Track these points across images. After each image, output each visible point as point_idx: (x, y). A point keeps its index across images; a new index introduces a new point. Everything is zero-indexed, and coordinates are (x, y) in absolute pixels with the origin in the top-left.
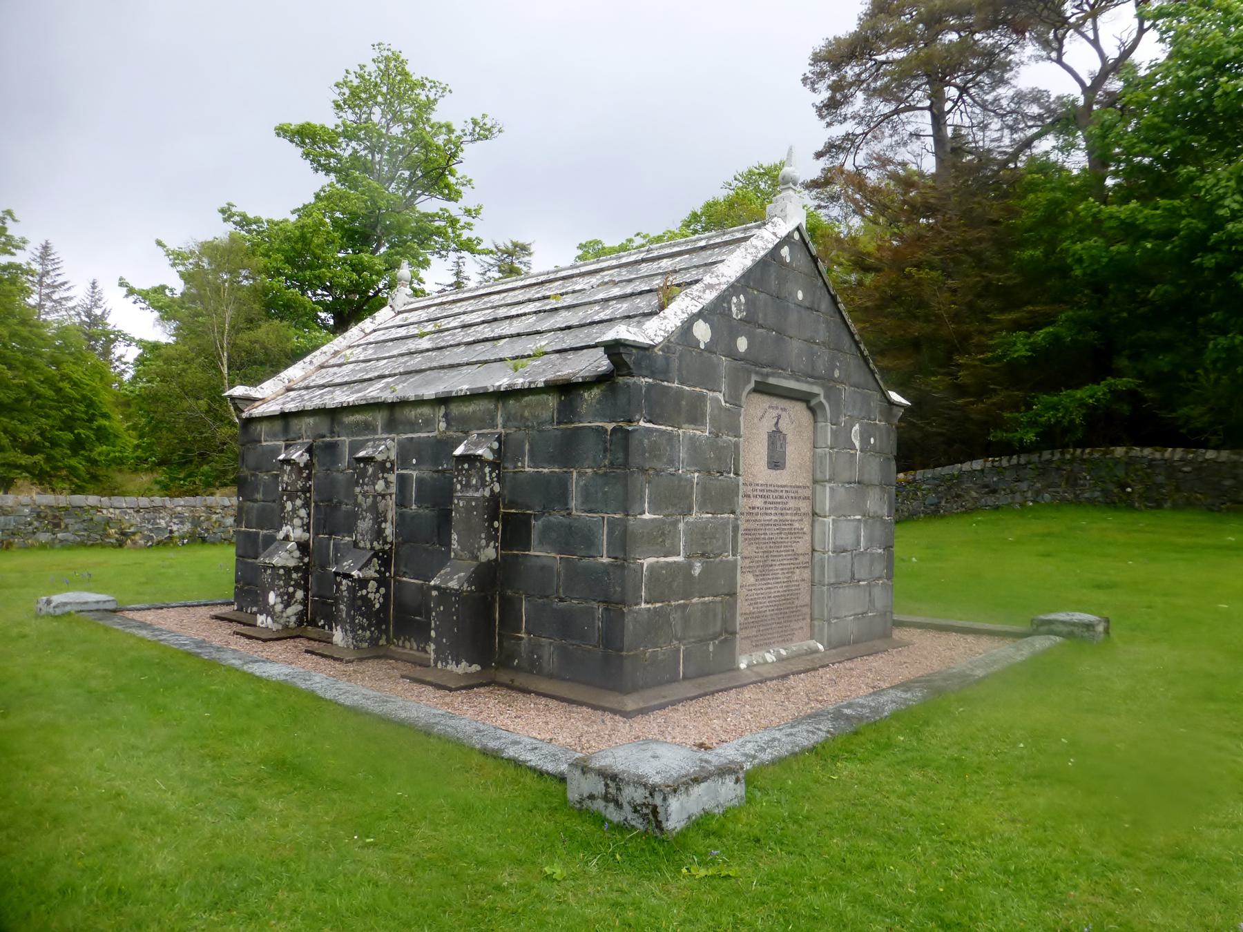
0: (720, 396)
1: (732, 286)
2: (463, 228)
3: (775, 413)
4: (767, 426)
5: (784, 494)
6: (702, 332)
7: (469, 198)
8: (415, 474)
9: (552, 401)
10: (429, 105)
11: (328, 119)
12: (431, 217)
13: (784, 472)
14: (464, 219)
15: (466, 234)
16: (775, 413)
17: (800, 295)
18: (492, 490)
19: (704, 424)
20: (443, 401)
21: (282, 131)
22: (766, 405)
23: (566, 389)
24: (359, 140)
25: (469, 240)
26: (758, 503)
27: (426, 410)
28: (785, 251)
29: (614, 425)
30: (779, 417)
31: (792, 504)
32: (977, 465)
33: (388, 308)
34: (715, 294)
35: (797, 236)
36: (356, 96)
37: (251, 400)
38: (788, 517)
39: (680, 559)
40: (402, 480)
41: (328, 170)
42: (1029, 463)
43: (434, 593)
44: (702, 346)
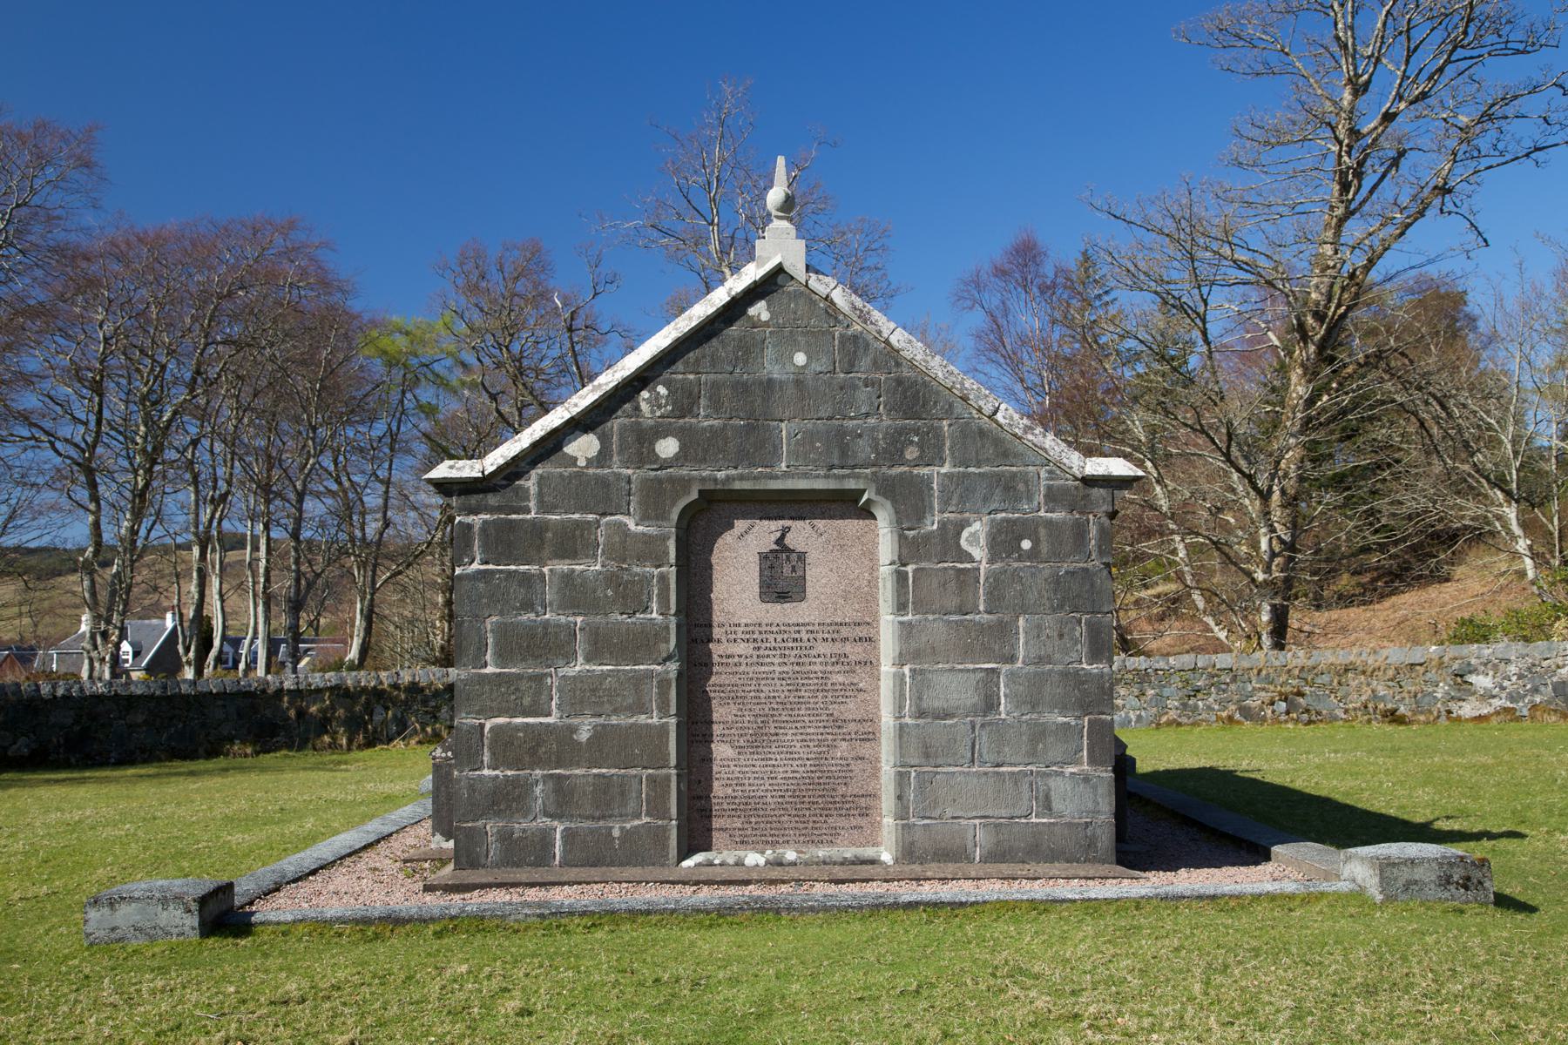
13: (803, 605)
31: (822, 648)
38: (817, 668)
44: (582, 463)
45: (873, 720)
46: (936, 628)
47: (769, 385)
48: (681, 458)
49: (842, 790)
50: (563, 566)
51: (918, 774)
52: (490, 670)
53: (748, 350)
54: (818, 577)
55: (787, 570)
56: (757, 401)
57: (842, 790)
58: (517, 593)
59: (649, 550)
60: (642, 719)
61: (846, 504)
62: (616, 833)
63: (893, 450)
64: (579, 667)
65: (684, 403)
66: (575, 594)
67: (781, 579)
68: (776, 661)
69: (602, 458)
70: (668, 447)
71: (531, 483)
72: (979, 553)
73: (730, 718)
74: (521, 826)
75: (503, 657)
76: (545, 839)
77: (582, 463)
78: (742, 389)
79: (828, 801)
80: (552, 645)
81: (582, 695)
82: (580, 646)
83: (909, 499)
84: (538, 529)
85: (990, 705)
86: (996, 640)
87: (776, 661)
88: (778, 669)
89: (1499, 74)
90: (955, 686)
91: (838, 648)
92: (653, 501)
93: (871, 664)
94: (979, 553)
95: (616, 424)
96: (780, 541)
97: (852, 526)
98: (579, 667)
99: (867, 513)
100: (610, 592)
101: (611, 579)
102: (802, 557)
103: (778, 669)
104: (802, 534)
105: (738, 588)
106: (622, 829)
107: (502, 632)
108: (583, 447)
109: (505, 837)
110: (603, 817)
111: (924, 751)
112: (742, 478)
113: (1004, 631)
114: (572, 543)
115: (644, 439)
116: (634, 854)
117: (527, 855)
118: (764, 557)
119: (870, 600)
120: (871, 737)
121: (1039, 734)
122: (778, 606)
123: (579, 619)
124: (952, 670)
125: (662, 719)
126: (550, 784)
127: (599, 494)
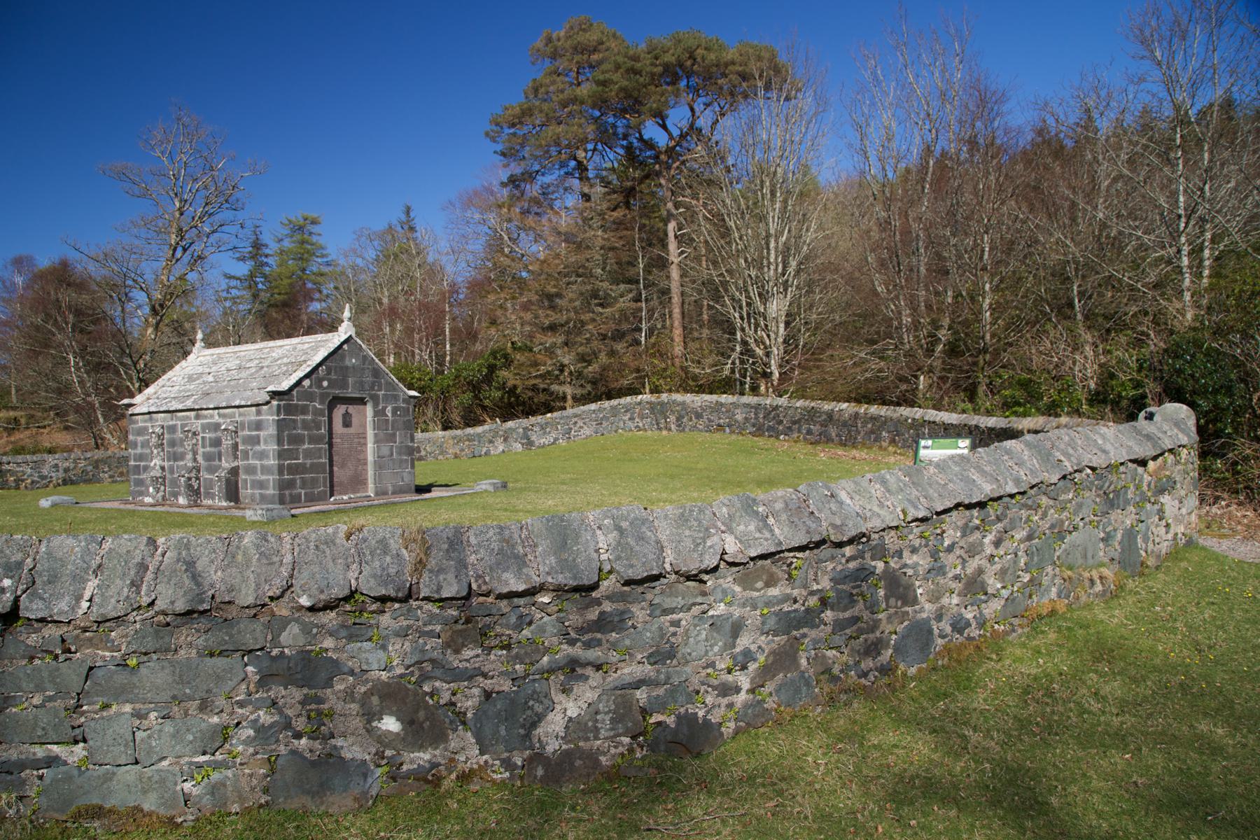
45: (366, 459)
46: (381, 434)
47: (347, 367)
48: (328, 387)
53: (343, 358)
54: (355, 421)
56: (344, 371)
59: (321, 413)
61: (361, 401)
63: (372, 388)
64: (306, 446)
65: (329, 371)
66: (306, 425)
67: (347, 423)
69: (310, 387)
70: (325, 384)
71: (294, 393)
74: (295, 492)
76: (300, 494)
78: (342, 368)
79: (358, 482)
81: (308, 454)
82: (570, 402)
83: (375, 399)
84: (297, 406)
85: (392, 454)
86: (392, 438)
89: (226, 215)
90: (385, 450)
92: (323, 397)
93: (365, 444)
95: (314, 376)
97: (361, 407)
98: (306, 446)
99: (365, 404)
101: (313, 421)
104: (352, 409)
107: (289, 436)
108: (307, 383)
109: (291, 495)
111: (379, 466)
113: (394, 435)
114: (304, 410)
115: (320, 380)
116: (321, 498)
117: (296, 500)
119: (365, 427)
120: (366, 464)
121: (401, 461)
125: (325, 460)
127: (309, 396)
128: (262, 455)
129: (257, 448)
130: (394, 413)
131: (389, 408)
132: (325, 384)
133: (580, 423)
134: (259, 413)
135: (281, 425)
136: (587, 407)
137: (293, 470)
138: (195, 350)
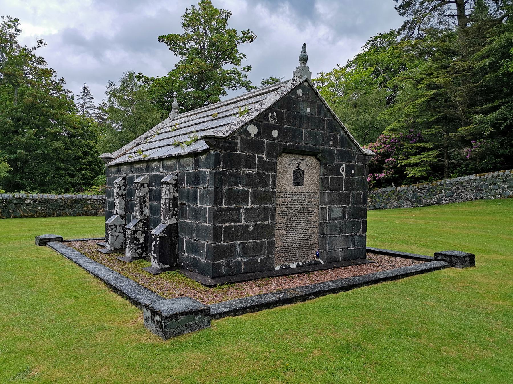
0: (264, 156)
1: (269, 108)
2: (243, 77)
3: (297, 162)
4: (293, 167)
5: (303, 196)
6: (253, 130)
7: (244, 63)
8: (154, 188)
9: (192, 160)
10: (225, 22)
11: (180, 31)
12: (228, 72)
13: (303, 186)
14: (243, 73)
15: (244, 80)
16: (297, 162)
17: (309, 110)
18: (174, 195)
19: (255, 168)
20: (161, 159)
21: (161, 38)
22: (292, 159)
23: (194, 155)
24: (194, 40)
25: (246, 82)
26: (288, 200)
27: (157, 163)
28: (299, 92)
29: (210, 170)
30: (299, 163)
31: (307, 200)
32: (473, 177)
33: (169, 118)
34: (258, 113)
35: (306, 84)
36: (191, 20)
37: (111, 159)
38: (305, 206)
39: (243, 223)
40: (151, 190)
41: (181, 54)
42: (499, 176)
43: (153, 236)
44: (253, 136)
49: (310, 242)
50: (247, 170)
51: (330, 237)
52: (224, 206)
55: (299, 175)
57: (310, 242)
58: (233, 180)
60: (266, 222)
62: (259, 261)
66: (250, 181)
68: (296, 204)
70: (275, 133)
72: (343, 173)
73: (285, 222)
74: (232, 261)
75: (229, 203)
77: (253, 136)
80: (243, 197)
87: (296, 204)
88: (296, 206)
91: (310, 200)
94: (343, 173)
96: (298, 167)
99: (215, 204)
100: (259, 181)
101: (259, 174)
102: (303, 172)
103: (296, 206)
105: (288, 181)
106: (261, 259)
109: (228, 264)
110: (256, 256)
112: (428, 132)
113: (347, 196)
114: (249, 163)
118: (294, 171)
122: (297, 187)
123: (250, 189)
124: (338, 207)
126: (241, 246)
128: (197, 214)
129: (193, 205)
130: (348, 173)
131: (344, 166)
132: (275, 133)
133: (461, 189)
134: (197, 163)
135: (219, 179)
136: (467, 178)
137: (230, 233)
138: (171, 115)
